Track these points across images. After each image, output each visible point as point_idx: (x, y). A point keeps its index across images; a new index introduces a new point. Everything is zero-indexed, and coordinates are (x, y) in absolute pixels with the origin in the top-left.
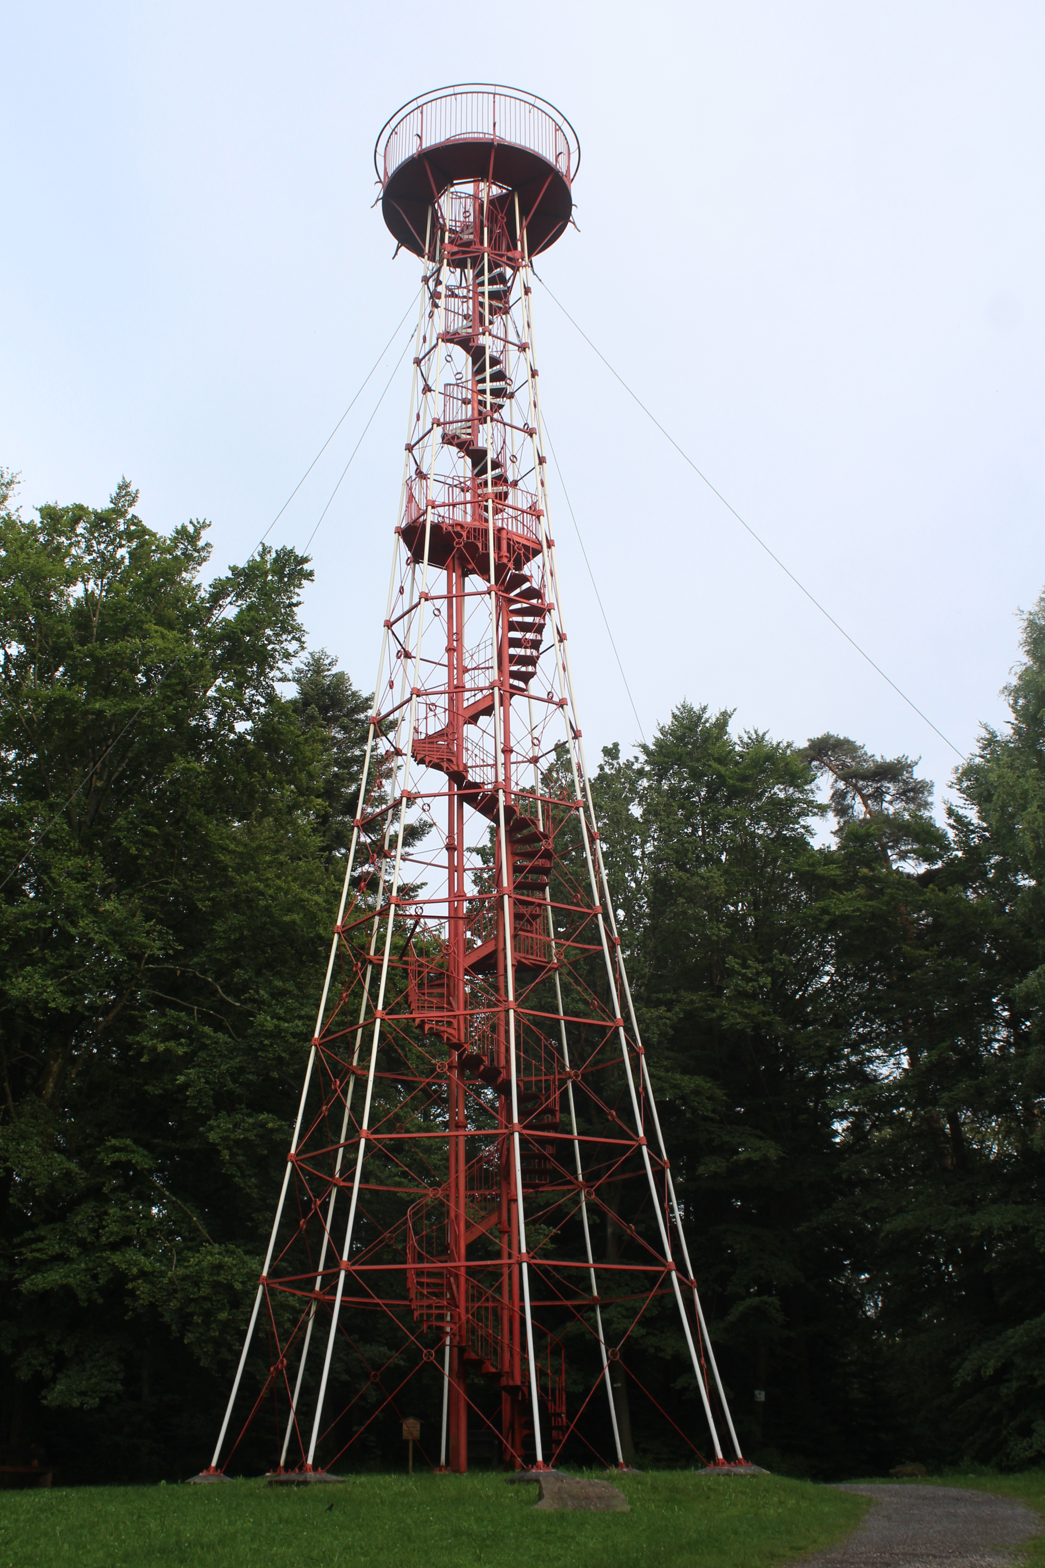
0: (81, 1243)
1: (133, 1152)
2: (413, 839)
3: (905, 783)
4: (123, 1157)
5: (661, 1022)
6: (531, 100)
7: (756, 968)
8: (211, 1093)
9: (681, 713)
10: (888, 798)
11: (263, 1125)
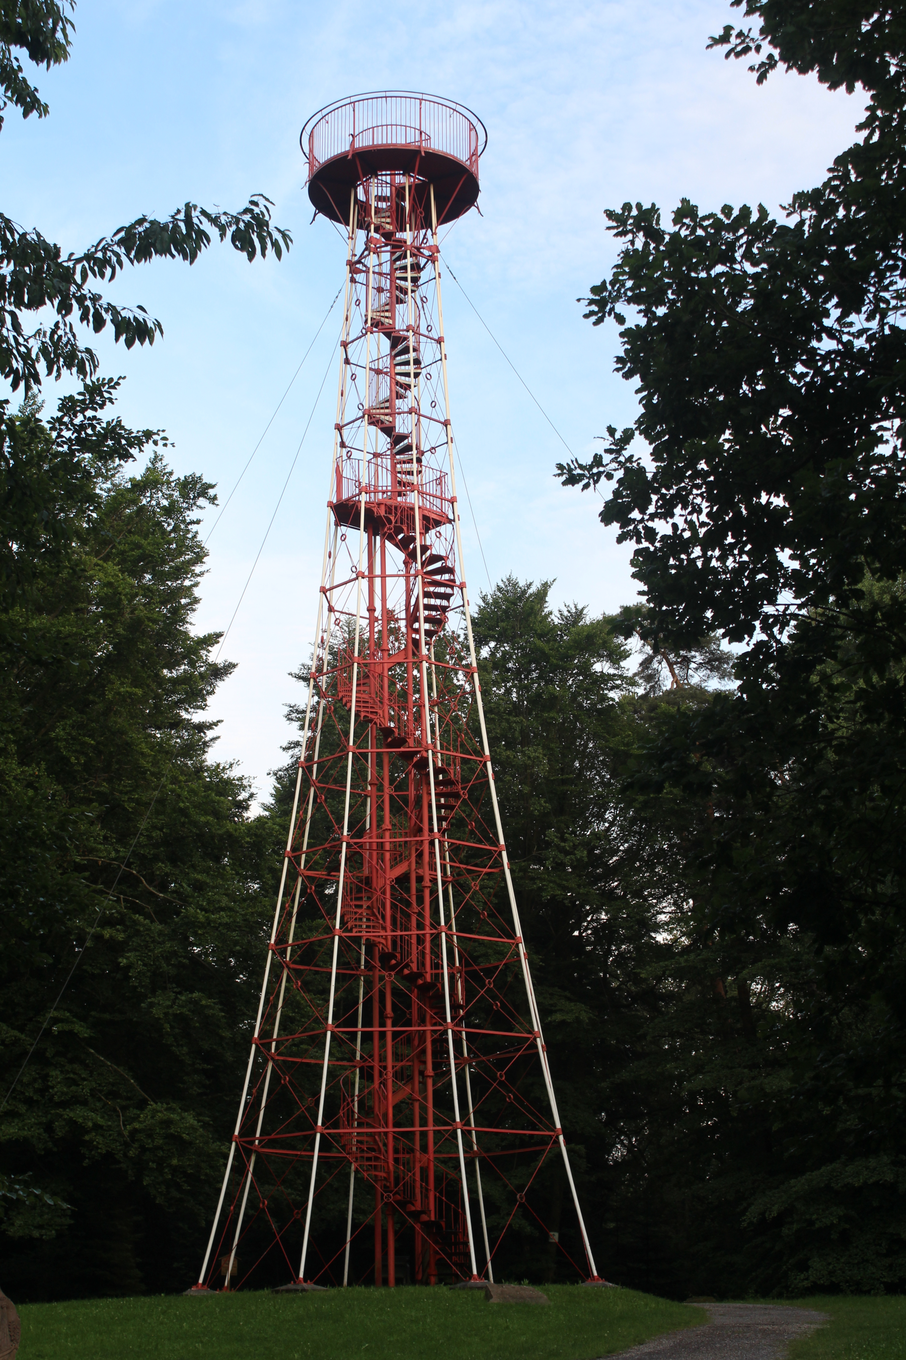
0: (29, 1102)
1: (73, 1022)
2: (216, 678)
3: (711, 653)
4: (66, 1027)
5: (485, 891)
6: (453, 106)
7: (572, 841)
8: (149, 974)
9: (506, 586)
10: (693, 665)
11: (196, 1003)
